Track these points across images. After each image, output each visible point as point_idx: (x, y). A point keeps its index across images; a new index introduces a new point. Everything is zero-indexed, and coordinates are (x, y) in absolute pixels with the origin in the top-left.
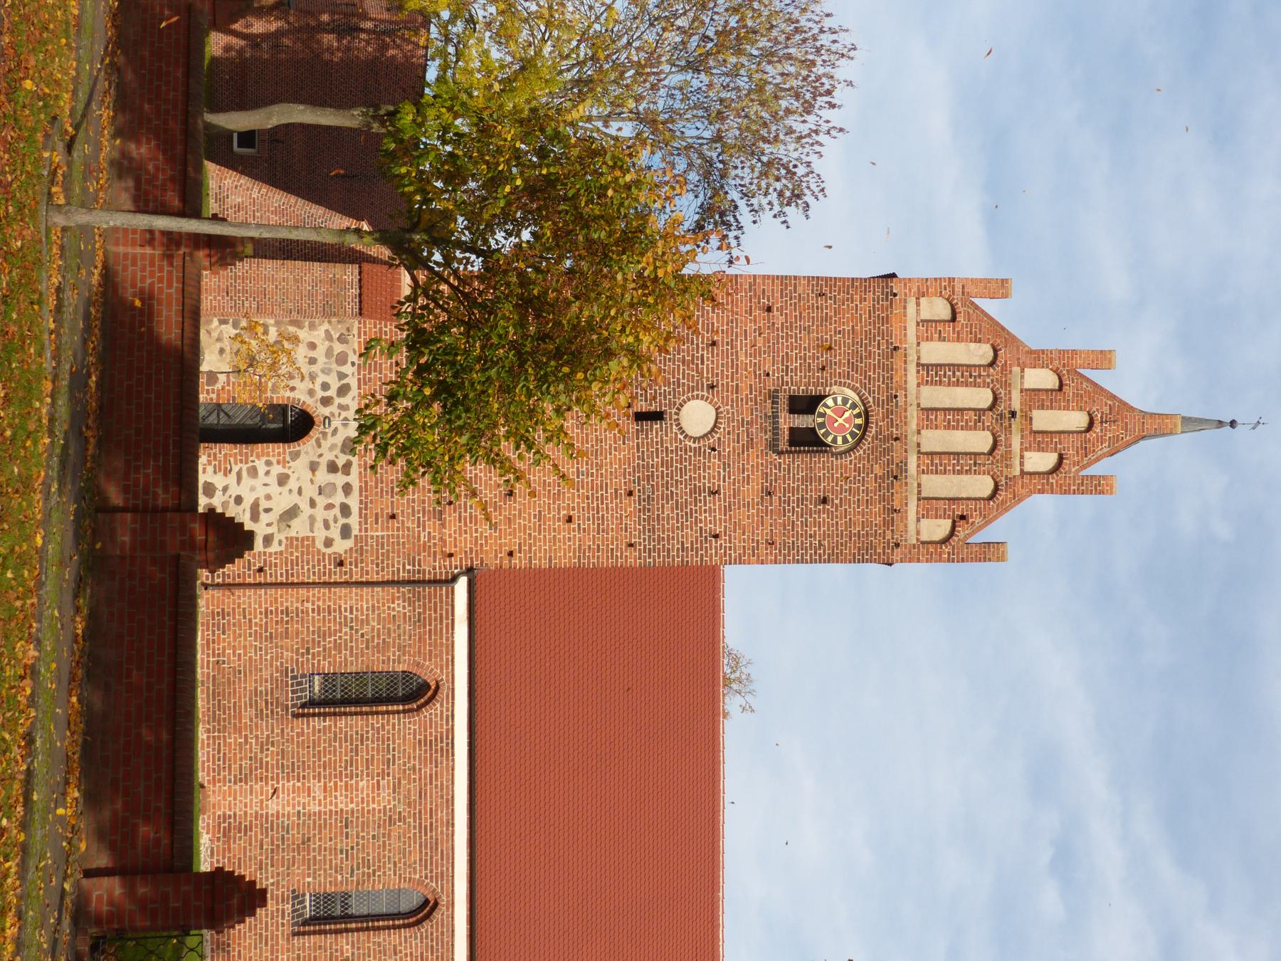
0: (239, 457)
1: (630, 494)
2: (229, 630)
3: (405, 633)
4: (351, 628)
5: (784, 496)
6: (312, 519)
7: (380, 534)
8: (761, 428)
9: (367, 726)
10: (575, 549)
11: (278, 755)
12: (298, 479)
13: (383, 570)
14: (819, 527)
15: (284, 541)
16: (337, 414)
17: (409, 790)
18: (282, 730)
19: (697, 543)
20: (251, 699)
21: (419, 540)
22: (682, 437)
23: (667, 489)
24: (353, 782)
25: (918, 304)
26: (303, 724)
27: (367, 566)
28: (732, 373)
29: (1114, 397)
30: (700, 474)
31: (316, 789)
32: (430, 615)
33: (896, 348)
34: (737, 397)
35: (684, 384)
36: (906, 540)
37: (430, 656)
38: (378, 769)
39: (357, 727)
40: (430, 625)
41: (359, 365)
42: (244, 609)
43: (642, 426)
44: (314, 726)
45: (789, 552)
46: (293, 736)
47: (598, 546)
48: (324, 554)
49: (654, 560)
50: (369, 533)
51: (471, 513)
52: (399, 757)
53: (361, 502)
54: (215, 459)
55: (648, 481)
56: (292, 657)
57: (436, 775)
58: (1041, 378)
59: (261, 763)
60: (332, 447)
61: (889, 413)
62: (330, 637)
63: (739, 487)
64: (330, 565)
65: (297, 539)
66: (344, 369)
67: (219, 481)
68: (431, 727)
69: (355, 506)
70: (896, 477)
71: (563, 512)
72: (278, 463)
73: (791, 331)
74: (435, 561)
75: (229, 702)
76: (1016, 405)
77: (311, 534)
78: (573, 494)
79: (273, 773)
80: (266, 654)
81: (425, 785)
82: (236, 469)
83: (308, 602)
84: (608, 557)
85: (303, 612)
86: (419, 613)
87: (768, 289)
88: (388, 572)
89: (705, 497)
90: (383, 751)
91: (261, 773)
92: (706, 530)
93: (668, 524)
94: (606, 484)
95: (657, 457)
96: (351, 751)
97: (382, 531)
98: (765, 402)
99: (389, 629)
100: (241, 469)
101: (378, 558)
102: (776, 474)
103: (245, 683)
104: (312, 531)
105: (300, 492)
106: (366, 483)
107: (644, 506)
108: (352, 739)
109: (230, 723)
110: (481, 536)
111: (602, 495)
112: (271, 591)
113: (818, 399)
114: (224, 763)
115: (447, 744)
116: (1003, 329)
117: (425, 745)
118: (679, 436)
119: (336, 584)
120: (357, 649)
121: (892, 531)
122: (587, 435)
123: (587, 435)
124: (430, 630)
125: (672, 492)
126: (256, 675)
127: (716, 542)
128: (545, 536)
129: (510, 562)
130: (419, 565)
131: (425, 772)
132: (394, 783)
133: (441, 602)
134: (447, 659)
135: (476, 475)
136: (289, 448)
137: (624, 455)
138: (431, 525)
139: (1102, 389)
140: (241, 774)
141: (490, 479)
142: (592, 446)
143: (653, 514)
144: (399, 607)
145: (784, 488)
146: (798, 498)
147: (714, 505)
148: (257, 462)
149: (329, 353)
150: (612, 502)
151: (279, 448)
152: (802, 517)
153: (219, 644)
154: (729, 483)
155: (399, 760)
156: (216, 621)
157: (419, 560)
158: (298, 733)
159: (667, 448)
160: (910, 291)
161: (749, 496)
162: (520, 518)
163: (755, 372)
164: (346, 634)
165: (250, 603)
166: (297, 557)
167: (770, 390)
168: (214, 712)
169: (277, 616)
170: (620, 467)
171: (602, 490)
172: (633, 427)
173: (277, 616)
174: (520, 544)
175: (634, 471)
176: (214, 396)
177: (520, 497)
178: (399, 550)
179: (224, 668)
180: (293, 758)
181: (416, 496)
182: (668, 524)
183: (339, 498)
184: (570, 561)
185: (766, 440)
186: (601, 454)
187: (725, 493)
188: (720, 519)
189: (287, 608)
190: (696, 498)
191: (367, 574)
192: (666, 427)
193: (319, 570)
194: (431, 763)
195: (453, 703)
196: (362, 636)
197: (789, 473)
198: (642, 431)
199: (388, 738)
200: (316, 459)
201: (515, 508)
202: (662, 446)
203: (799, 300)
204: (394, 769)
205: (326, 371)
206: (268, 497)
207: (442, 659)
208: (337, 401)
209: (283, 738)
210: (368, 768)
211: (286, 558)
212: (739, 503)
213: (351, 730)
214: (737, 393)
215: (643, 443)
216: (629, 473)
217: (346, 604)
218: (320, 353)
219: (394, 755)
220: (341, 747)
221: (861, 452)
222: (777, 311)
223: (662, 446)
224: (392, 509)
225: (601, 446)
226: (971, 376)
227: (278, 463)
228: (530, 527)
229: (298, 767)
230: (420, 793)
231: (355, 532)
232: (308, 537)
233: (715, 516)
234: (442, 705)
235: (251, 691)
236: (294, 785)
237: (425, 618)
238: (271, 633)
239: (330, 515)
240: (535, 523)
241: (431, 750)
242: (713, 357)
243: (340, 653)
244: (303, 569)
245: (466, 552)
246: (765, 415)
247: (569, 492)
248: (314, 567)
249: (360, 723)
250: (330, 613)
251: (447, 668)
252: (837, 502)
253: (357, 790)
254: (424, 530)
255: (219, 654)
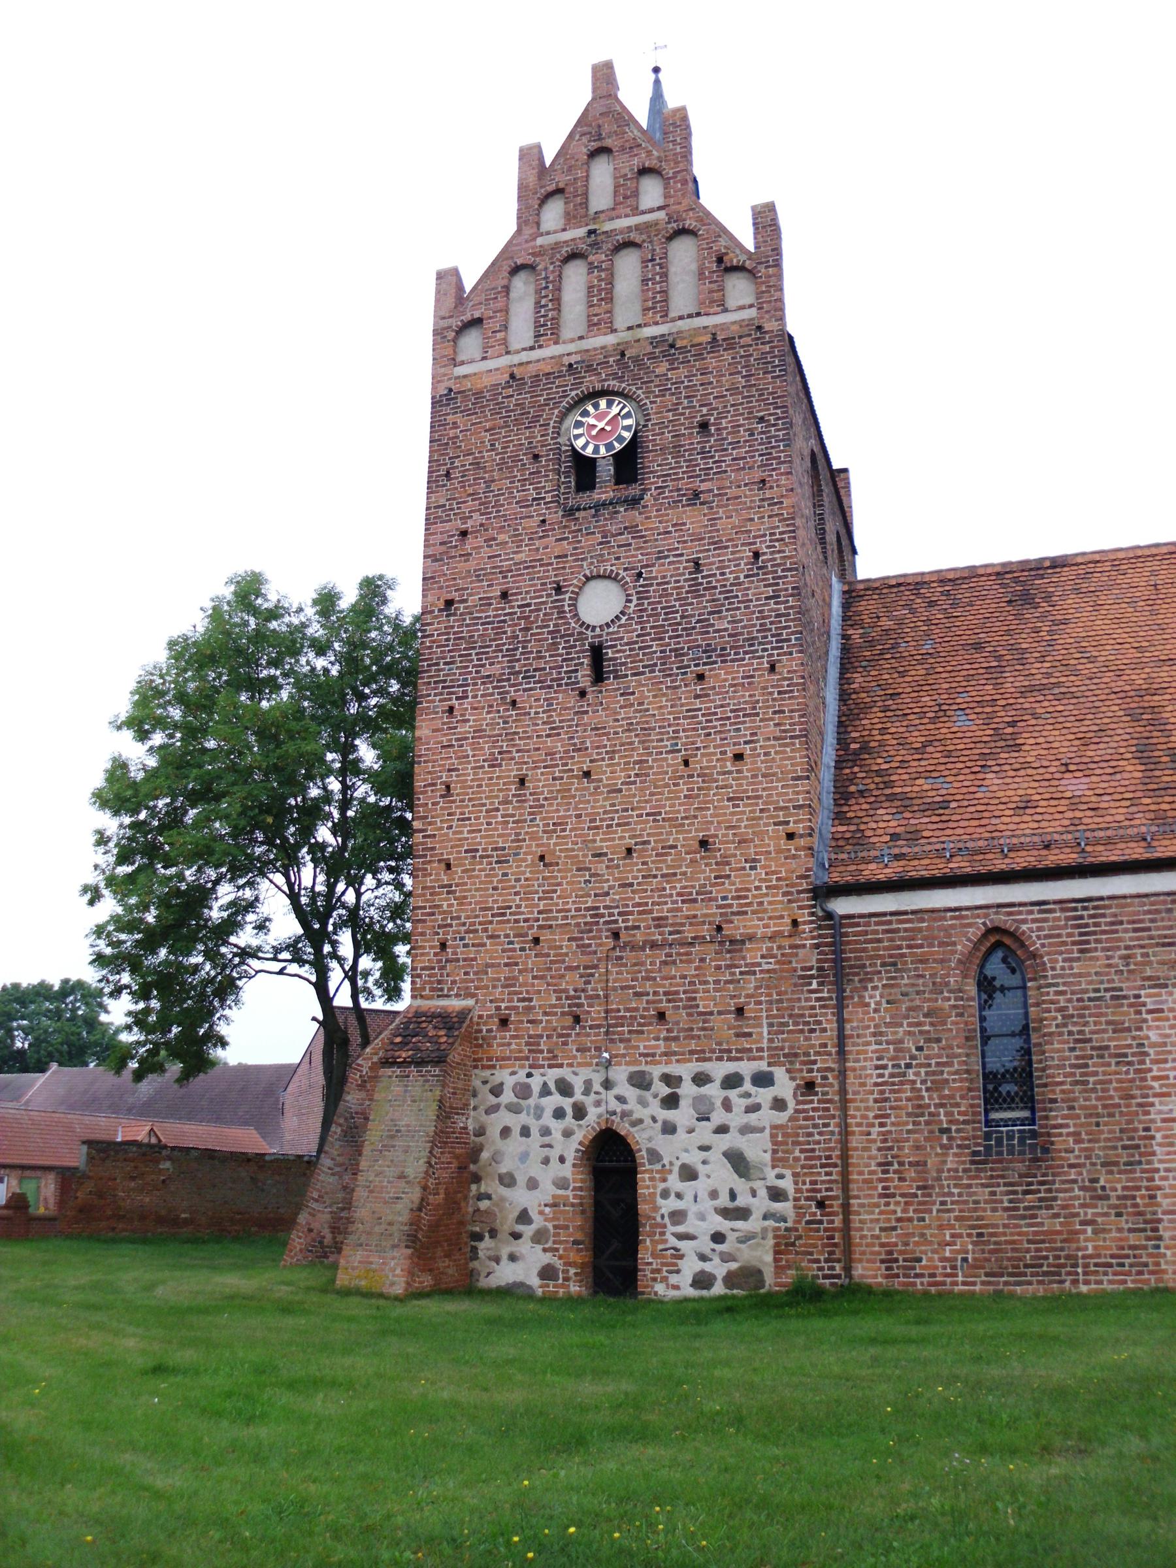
0: (657, 1237)
1: (701, 677)
2: (914, 1252)
3: (913, 985)
4: (908, 1066)
5: (700, 476)
6: (746, 1130)
7: (765, 1030)
8: (611, 519)
9: (1061, 1034)
10: (780, 745)
11: (1111, 1172)
12: (686, 1151)
13: (819, 1023)
14: (739, 426)
15: (777, 1171)
16: (598, 1097)
17: (1163, 963)
18: (1071, 1166)
19: (768, 579)
20: (1024, 1217)
21: (773, 970)
22: (624, 618)
23: (694, 628)
24: (1151, 1051)
25: (462, 363)
26: (1060, 1135)
27: (813, 1046)
28: (541, 565)
29: (571, 136)
30: (673, 588)
31: (1165, 1108)
32: (885, 949)
33: (512, 376)
34: (572, 555)
35: (555, 625)
36: (753, 319)
37: (948, 944)
38: (1128, 1014)
39: (1063, 1050)
40: (900, 947)
41: (531, 1067)
42: (881, 1229)
43: (609, 672)
44: (1065, 1117)
45: (775, 458)
46: (1081, 1150)
47: (775, 713)
48: (797, 1111)
49: (793, 633)
50: (765, 1045)
51: (733, 898)
52: (1109, 981)
53: (720, 1059)
54: (658, 1271)
55: (683, 655)
56: (955, 1155)
57: (1134, 922)
58: (553, 214)
59: (1125, 1198)
60: (643, 1103)
61: (590, 369)
62: (922, 1098)
63: (689, 535)
64: (812, 1102)
65: (775, 1152)
66: (536, 1087)
67: (690, 1266)
68: (1059, 936)
69: (729, 1067)
70: (672, 346)
71: (729, 766)
72: (664, 1180)
73: (490, 502)
74: (804, 946)
75: (1028, 1251)
76: (581, 232)
77: (767, 1131)
78: (703, 755)
79: (1141, 1179)
80: (951, 1194)
81: (1151, 938)
82: (673, 1241)
83: (869, 1134)
84: (790, 698)
85: (885, 1141)
86: (883, 965)
87: (439, 538)
88: (823, 1015)
89: (703, 577)
90: (1099, 1007)
91: (1142, 1197)
92: (749, 570)
93: (741, 621)
94: (688, 711)
95: (651, 647)
96: (1102, 1057)
97: (761, 1026)
98: (577, 519)
99: (909, 1009)
100: (673, 1234)
101: (802, 1031)
102: (671, 491)
103: (996, 1226)
104: (762, 1130)
105: (705, 1148)
106: (692, 1052)
107: (717, 656)
108: (1083, 1057)
109: (1062, 1249)
110: (765, 880)
111: (703, 715)
112: (854, 1189)
113: (577, 457)
114: (1127, 1256)
115: (1085, 908)
116: (493, 264)
117: (1088, 942)
118: (623, 621)
119: (843, 1091)
120: (940, 1056)
121: (740, 337)
122: (622, 745)
123: (622, 745)
124: (909, 947)
125: (698, 622)
126: (984, 1210)
127: (764, 554)
128: (764, 789)
129: (801, 836)
130: (811, 968)
131: (1131, 939)
132: (1150, 987)
133: (866, 933)
134: (953, 918)
135: (679, 894)
136: (643, 1165)
137: (649, 691)
138: (753, 954)
139: (563, 147)
140: (1144, 1230)
141: (685, 873)
142: (636, 736)
143: (728, 642)
144: (874, 997)
145: (689, 477)
146: (702, 458)
147: (713, 563)
148: (663, 1211)
149: (514, 1109)
150: (714, 701)
151: (643, 1180)
152: (726, 450)
153: (936, 1268)
154: (684, 548)
155: (1113, 981)
156: (901, 1272)
157: (803, 969)
158: (1076, 1142)
159: (638, 636)
160: (445, 375)
161: (700, 521)
162: (739, 827)
163: (541, 538)
164: (917, 1074)
165: (872, 1221)
166: (802, 1151)
167: (563, 516)
168: (1045, 1274)
169: (892, 1180)
170: (664, 695)
171: (696, 716)
172: (611, 683)
173: (892, 1180)
174: (775, 824)
175: (670, 675)
176: (572, 1271)
177: (709, 830)
178: (789, 1000)
179: (974, 1259)
180: (1115, 1148)
181: (710, 979)
182: (741, 621)
183: (713, 1091)
184: (798, 750)
185: (626, 510)
186: (647, 722)
187: (698, 552)
188: (733, 553)
189: (879, 1164)
190: (705, 589)
191: (825, 1045)
192: (611, 640)
193: (820, 1118)
194: (1116, 932)
195: (1021, 904)
196: (920, 1049)
197: (669, 475)
198: (616, 671)
199: (1079, 1000)
200: (659, 1125)
201: (724, 835)
202: (636, 642)
203: (454, 499)
204: (1129, 988)
205: (539, 1112)
206: (714, 1195)
207: (952, 927)
208: (578, 1096)
209: (1084, 1165)
210: (1129, 1030)
211: (803, 1167)
212: (710, 532)
213: (1069, 1058)
214: (566, 556)
215: (632, 668)
216: (672, 681)
217: (871, 1076)
218: (514, 1122)
219: (1106, 990)
220: (1095, 1074)
221: (640, 392)
222: (466, 523)
223: (636, 642)
224: (729, 1012)
225: (638, 723)
226: (546, 288)
227: (664, 1180)
228: (751, 812)
229: (1130, 1139)
230: (1164, 945)
231: (763, 1066)
232: (773, 1136)
233: (729, 560)
234: (1024, 921)
235: (1010, 1217)
236: (1160, 1145)
237: (891, 956)
238: (918, 1188)
239: (739, 1104)
240: (745, 805)
241: (1094, 933)
242: (521, 593)
243: (947, 1081)
244: (819, 1143)
245: (790, 901)
246: (594, 516)
247: (700, 762)
248: (815, 1126)
249: (1056, 1046)
250: (886, 1100)
251: (966, 917)
252: (705, 410)
253: (1165, 1044)
254: (759, 965)
255: (954, 1267)
